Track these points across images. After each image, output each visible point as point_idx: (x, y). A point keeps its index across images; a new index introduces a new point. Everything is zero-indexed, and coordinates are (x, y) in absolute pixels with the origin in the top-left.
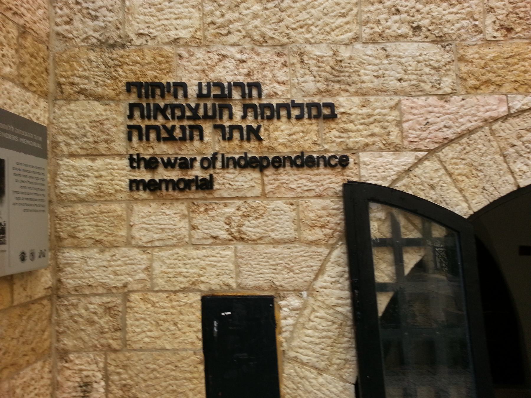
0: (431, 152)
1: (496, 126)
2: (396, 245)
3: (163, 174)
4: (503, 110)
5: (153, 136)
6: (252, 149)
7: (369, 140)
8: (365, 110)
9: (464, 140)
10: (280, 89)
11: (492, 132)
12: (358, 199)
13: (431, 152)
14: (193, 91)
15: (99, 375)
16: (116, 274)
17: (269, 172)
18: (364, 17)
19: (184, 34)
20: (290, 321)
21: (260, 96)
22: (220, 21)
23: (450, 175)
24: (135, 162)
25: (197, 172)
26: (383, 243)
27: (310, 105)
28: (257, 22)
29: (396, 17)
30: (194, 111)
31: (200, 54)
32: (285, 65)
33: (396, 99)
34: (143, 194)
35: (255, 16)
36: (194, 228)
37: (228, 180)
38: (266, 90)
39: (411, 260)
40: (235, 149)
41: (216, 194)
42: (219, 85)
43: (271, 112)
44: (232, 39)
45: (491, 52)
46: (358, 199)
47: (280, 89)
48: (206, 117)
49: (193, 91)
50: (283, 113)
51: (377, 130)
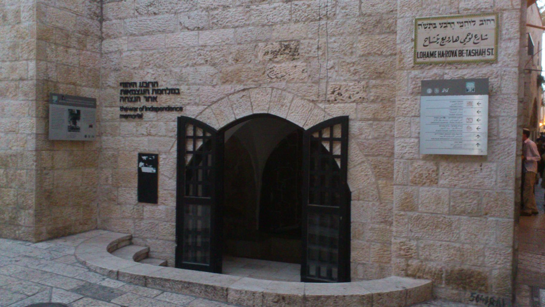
0: (209, 106)
1: (230, 97)
2: (195, 138)
3: (129, 113)
4: (233, 90)
5: (127, 100)
6: (155, 105)
7: (189, 102)
8: (188, 91)
9: (219, 102)
10: (164, 83)
11: (229, 99)
12: (183, 122)
13: (209, 106)
14: (138, 85)
15: (110, 176)
16: (116, 145)
17: (159, 112)
18: (190, 57)
19: (137, 66)
20: (162, 162)
21: (157, 86)
22: (147, 60)
23: (214, 114)
24: (122, 109)
25: (139, 112)
26: (190, 137)
27: (172, 89)
28: (158, 60)
29: (200, 57)
30: (138, 91)
31: (141, 72)
32: (166, 75)
33: (199, 86)
34: (123, 119)
35: (157, 58)
36: (137, 131)
37: (149, 115)
38: (159, 84)
39: (200, 144)
40: (149, 105)
41: (144, 120)
42: (146, 83)
43: (161, 92)
44: (150, 66)
45: (230, 69)
46: (183, 122)
47: (164, 83)
48: (141, 94)
49: (138, 85)
50: (164, 92)
51: (192, 98)
